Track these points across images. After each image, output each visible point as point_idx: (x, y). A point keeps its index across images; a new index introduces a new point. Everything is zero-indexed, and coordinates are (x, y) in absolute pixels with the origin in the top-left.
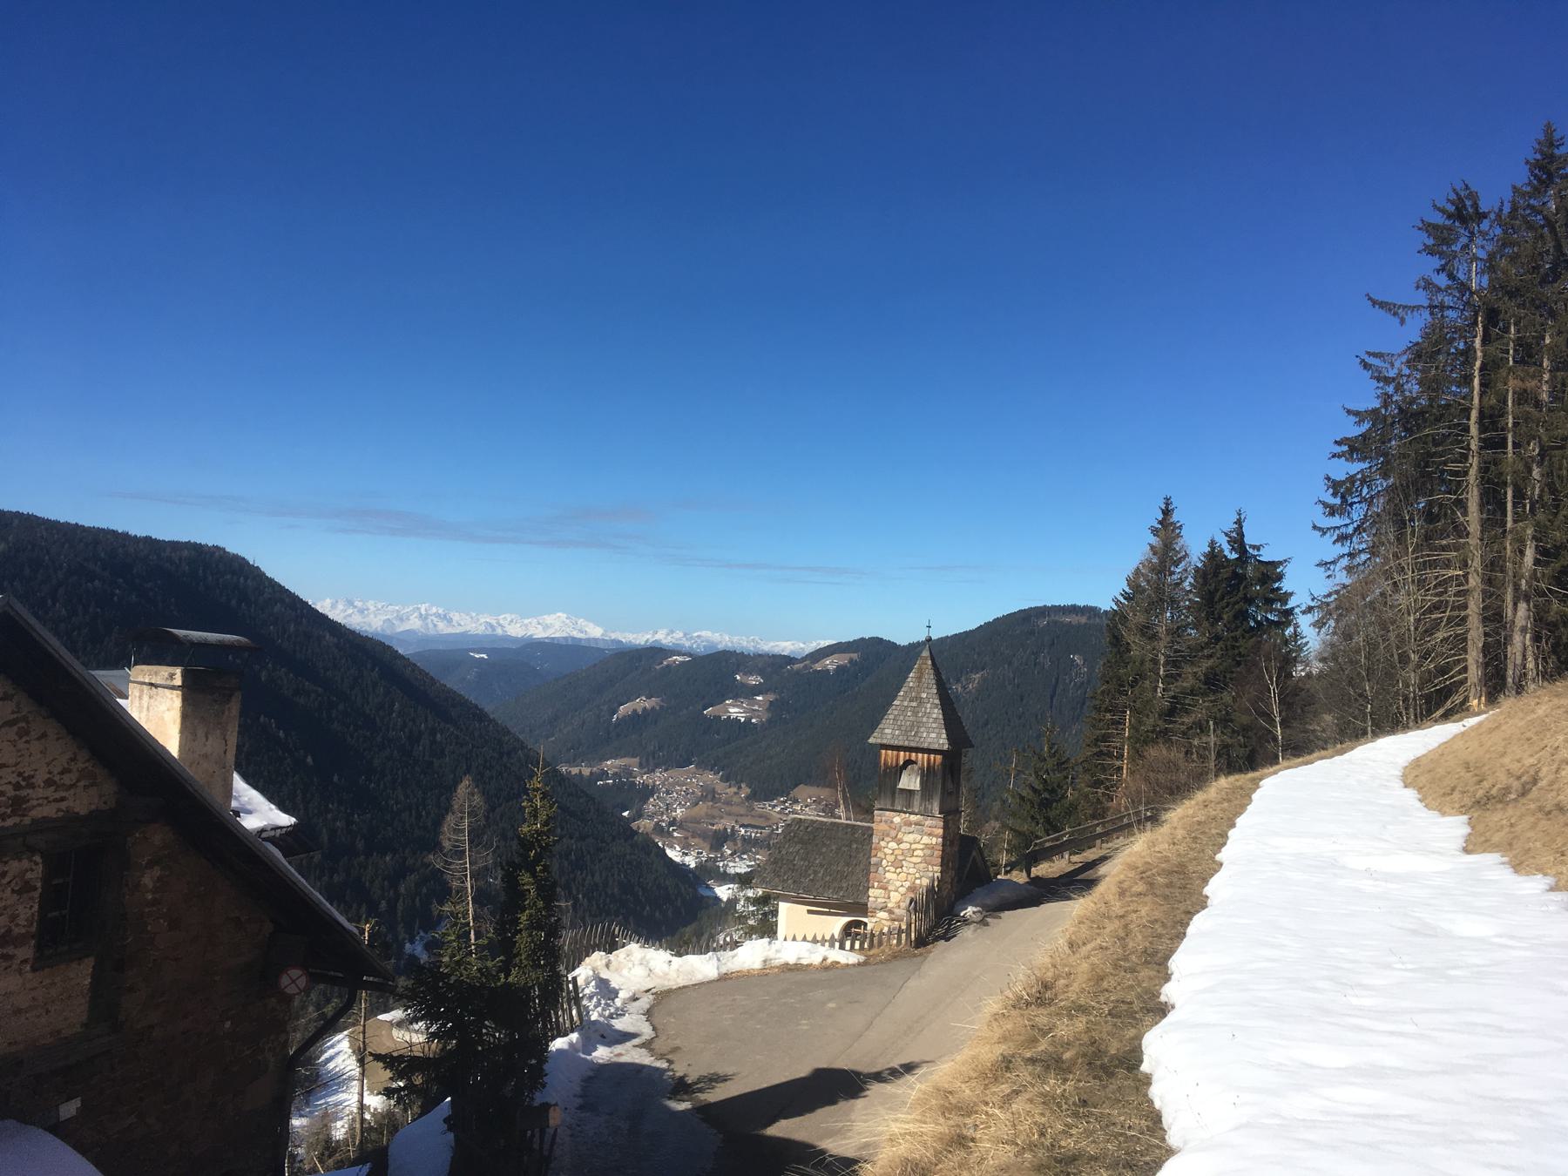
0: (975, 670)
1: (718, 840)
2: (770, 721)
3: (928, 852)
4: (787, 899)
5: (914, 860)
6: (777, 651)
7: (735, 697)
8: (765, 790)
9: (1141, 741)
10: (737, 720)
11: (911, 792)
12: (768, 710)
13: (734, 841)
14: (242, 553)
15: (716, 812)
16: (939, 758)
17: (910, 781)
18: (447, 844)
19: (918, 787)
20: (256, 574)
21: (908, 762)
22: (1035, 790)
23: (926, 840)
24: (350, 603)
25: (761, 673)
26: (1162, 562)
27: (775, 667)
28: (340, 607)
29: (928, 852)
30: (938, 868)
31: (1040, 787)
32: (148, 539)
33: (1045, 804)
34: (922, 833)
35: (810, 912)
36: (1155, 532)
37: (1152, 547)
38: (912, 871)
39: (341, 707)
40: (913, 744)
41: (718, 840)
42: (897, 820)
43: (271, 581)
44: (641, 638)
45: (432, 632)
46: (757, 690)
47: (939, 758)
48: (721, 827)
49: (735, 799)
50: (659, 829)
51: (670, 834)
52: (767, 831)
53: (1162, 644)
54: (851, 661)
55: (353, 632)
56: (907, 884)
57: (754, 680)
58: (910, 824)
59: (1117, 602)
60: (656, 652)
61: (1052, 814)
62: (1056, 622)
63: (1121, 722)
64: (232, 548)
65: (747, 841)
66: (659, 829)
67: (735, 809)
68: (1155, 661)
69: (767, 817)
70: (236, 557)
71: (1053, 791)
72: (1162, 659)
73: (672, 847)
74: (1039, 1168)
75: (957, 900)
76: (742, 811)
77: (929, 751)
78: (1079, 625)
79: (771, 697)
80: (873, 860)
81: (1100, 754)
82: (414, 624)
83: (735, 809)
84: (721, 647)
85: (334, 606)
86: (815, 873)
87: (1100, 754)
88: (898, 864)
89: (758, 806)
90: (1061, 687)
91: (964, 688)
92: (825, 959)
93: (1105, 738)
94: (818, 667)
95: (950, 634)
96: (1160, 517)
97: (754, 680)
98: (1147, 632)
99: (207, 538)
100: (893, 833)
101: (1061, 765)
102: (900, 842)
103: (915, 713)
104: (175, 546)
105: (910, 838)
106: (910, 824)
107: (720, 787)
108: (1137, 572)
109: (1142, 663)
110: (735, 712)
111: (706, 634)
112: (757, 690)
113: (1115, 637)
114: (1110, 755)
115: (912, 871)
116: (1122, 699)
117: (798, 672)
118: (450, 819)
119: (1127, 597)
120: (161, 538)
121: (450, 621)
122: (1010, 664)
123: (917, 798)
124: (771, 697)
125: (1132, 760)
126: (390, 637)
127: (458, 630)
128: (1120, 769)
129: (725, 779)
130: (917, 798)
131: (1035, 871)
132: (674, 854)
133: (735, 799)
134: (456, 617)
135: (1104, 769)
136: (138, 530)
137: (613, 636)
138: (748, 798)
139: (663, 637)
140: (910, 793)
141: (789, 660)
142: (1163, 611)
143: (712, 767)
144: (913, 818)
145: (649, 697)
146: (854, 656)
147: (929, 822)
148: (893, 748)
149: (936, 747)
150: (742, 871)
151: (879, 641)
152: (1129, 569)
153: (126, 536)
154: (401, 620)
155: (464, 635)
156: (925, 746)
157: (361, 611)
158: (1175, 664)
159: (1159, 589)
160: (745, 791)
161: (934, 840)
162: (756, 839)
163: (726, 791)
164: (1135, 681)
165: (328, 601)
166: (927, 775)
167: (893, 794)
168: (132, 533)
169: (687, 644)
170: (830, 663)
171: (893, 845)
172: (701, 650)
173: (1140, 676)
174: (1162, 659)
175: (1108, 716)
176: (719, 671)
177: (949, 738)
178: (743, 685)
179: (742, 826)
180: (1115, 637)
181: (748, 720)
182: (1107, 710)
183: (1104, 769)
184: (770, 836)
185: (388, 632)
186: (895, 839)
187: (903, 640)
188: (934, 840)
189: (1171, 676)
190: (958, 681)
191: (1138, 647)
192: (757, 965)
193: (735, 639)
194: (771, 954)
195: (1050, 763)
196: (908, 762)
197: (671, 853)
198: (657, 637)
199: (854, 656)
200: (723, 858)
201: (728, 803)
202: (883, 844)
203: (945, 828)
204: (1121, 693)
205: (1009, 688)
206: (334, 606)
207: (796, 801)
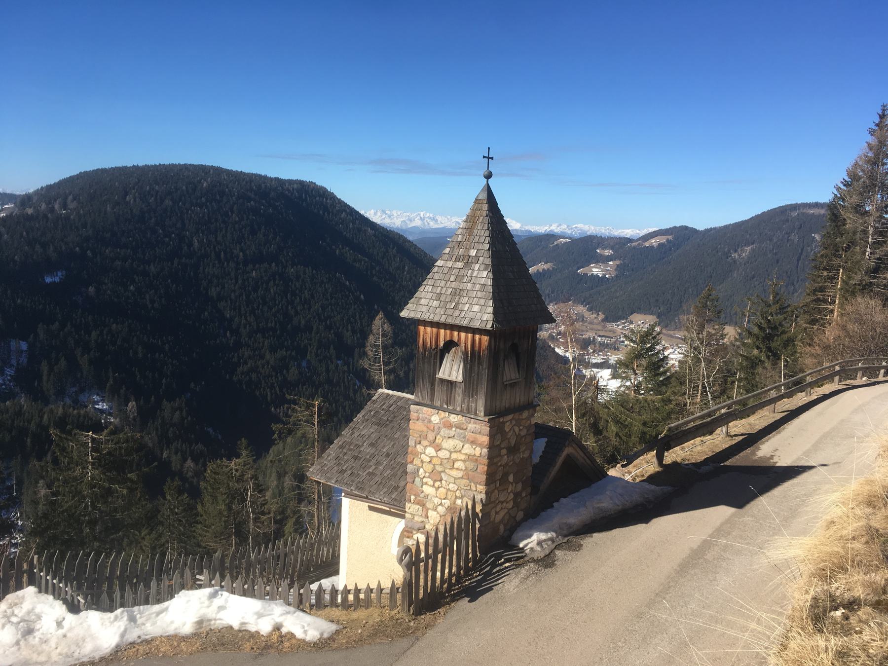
0: (747, 245)
1: (585, 344)
2: (617, 276)
3: (470, 465)
4: (349, 495)
5: (454, 473)
6: (622, 235)
7: (597, 262)
8: (613, 316)
9: (850, 292)
10: (597, 276)
11: (451, 384)
12: (616, 270)
13: (595, 344)
14: (324, 185)
15: (584, 328)
16: (485, 339)
17: (452, 370)
18: (370, 353)
19: (460, 379)
20: (332, 197)
21: (450, 345)
22: (760, 328)
23: (468, 449)
24: (384, 212)
25: (612, 248)
26: (877, 155)
27: (620, 245)
28: (379, 214)
29: (470, 465)
30: (482, 488)
31: (765, 325)
32: (277, 179)
33: (769, 338)
34: (465, 440)
35: (371, 508)
36: (872, 132)
37: (869, 144)
38: (452, 486)
39: (377, 269)
40: (450, 321)
41: (585, 344)
42: (435, 419)
43: (339, 200)
44: (542, 229)
45: (427, 227)
46: (609, 258)
47: (485, 339)
48: (587, 336)
49: (595, 321)
50: (551, 337)
51: (558, 340)
52: (613, 340)
53: (872, 219)
54: (667, 240)
55: (383, 228)
56: (447, 503)
57: (608, 252)
58: (449, 426)
59: (838, 189)
60: (550, 237)
61: (773, 345)
62: (803, 214)
63: (835, 277)
64: (319, 183)
65: (602, 345)
66: (551, 337)
67: (595, 326)
68: (865, 232)
69: (614, 332)
70: (321, 187)
71: (775, 328)
72: (871, 230)
73: (559, 347)
74: (884, 306)
75: (525, 519)
76: (600, 328)
77: (474, 331)
78: (820, 215)
79: (618, 262)
80: (410, 468)
81: (818, 300)
82: (417, 223)
83: (595, 326)
84: (589, 233)
85: (375, 214)
86: (378, 463)
87: (818, 300)
88: (436, 476)
89: (609, 325)
90: (804, 254)
91: (739, 255)
92: (277, 628)
93: (822, 289)
94: (647, 244)
95: (732, 222)
96: (877, 120)
97: (608, 252)
98: (858, 209)
99: (306, 177)
100: (431, 436)
101: (782, 309)
102: (438, 448)
103: (459, 278)
104: (291, 182)
105: (449, 444)
106: (449, 426)
107: (587, 314)
108: (856, 165)
109: (855, 233)
110: (596, 270)
111: (580, 226)
112: (609, 258)
113: (834, 214)
114: (825, 301)
115: (452, 486)
116: (836, 261)
117: (634, 247)
118: (371, 339)
119: (846, 184)
120: (283, 178)
121: (436, 221)
122: (770, 240)
123: (459, 392)
124: (618, 262)
125: (841, 306)
126: (405, 231)
127: (441, 226)
128: (832, 311)
129: (590, 309)
130: (459, 392)
131: (673, 456)
132: (559, 351)
133: (595, 321)
134: (439, 218)
135: (820, 311)
136: (272, 174)
137: (527, 228)
138: (603, 321)
139: (555, 228)
140: (450, 384)
141: (629, 240)
142: (875, 193)
143: (583, 302)
144: (454, 418)
145: (546, 263)
146: (670, 237)
147: (472, 426)
148: (433, 324)
149: (476, 324)
150: (599, 361)
151: (686, 228)
152: (849, 163)
153: (265, 177)
154: (411, 221)
155: (444, 228)
156: (465, 323)
157: (390, 216)
158: (881, 234)
159: (872, 177)
160: (601, 316)
161: (478, 451)
162: (607, 344)
163: (590, 316)
164: (848, 247)
165: (372, 211)
166: (471, 360)
167: (432, 384)
168: (269, 175)
169: (569, 232)
170: (654, 242)
171: (431, 451)
172: (577, 235)
173: (852, 243)
174: (871, 230)
175: (826, 273)
176: (587, 247)
177: (495, 313)
178: (601, 255)
179: (599, 336)
180: (834, 214)
181: (604, 276)
182: (825, 269)
183: (820, 311)
184: (615, 342)
185: (404, 227)
186: (433, 443)
187: (701, 227)
188: (478, 451)
189: (878, 243)
190: (736, 251)
191: (851, 221)
192: (187, 629)
193: (598, 228)
194: (210, 612)
195: (773, 309)
196: (450, 345)
197: (557, 350)
198: (552, 228)
199: (670, 237)
200: (588, 354)
201: (591, 323)
202: (419, 448)
203: (492, 436)
204: (836, 256)
205: (769, 256)
206: (375, 214)
207: (631, 323)
